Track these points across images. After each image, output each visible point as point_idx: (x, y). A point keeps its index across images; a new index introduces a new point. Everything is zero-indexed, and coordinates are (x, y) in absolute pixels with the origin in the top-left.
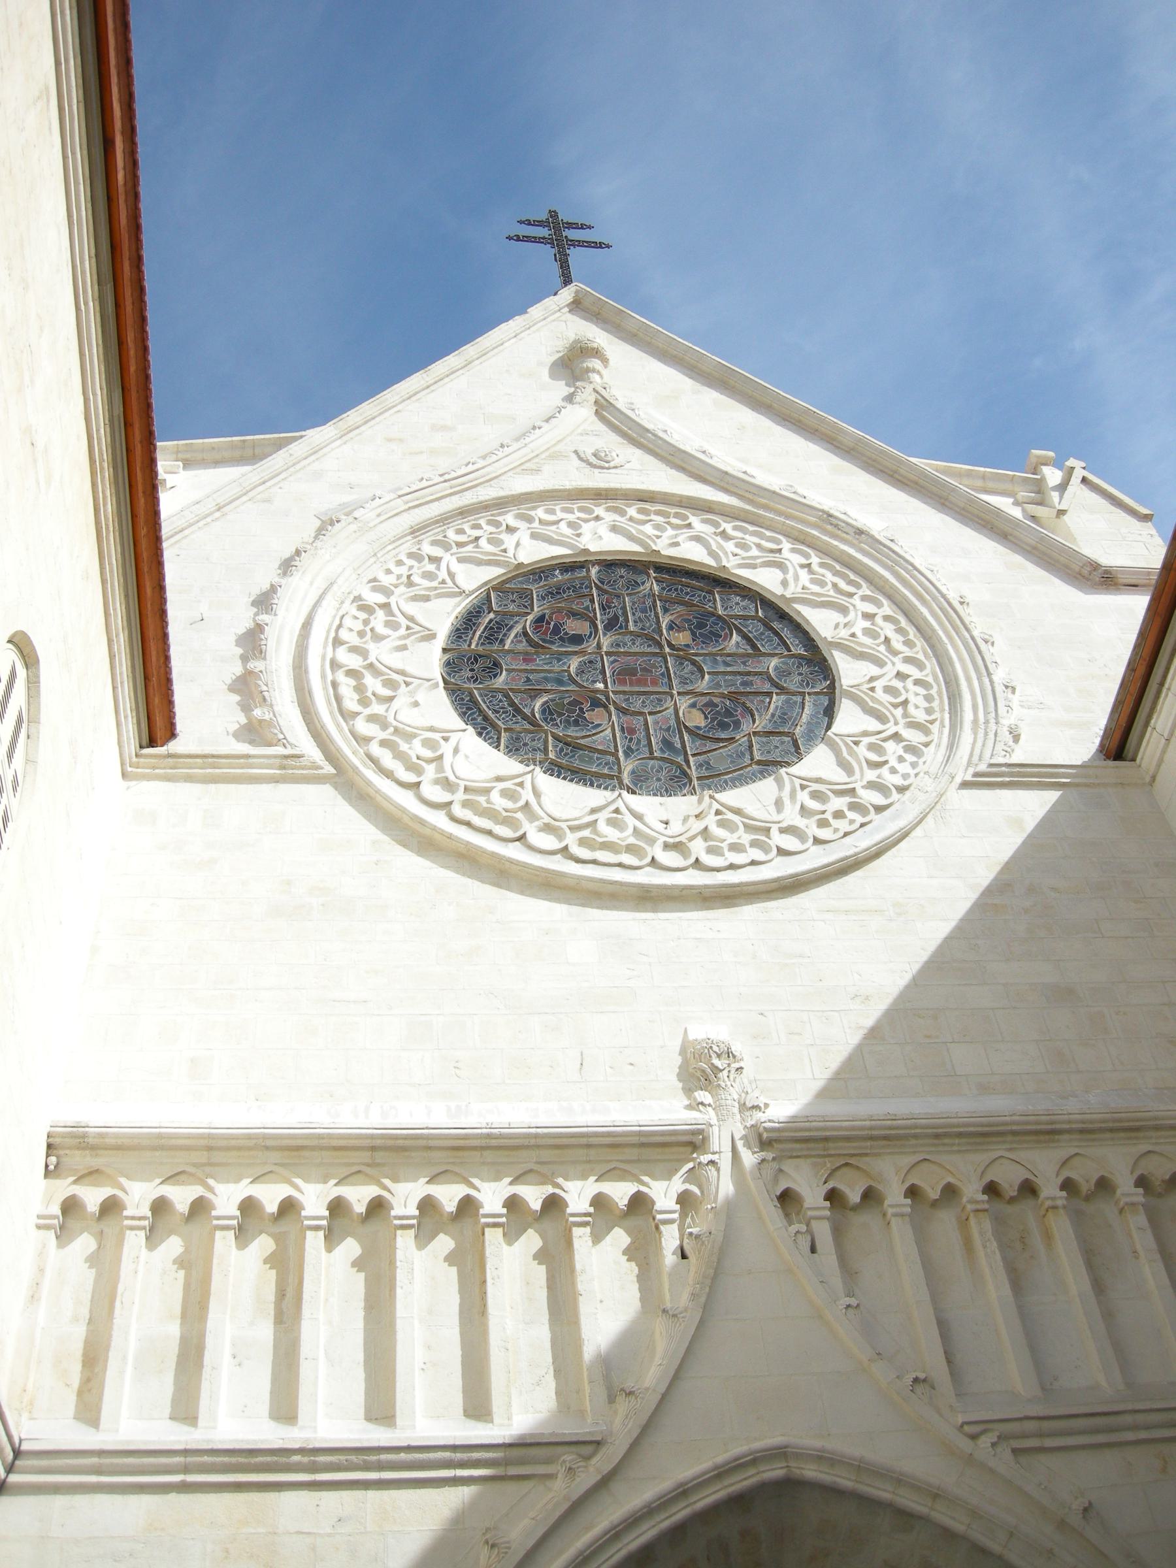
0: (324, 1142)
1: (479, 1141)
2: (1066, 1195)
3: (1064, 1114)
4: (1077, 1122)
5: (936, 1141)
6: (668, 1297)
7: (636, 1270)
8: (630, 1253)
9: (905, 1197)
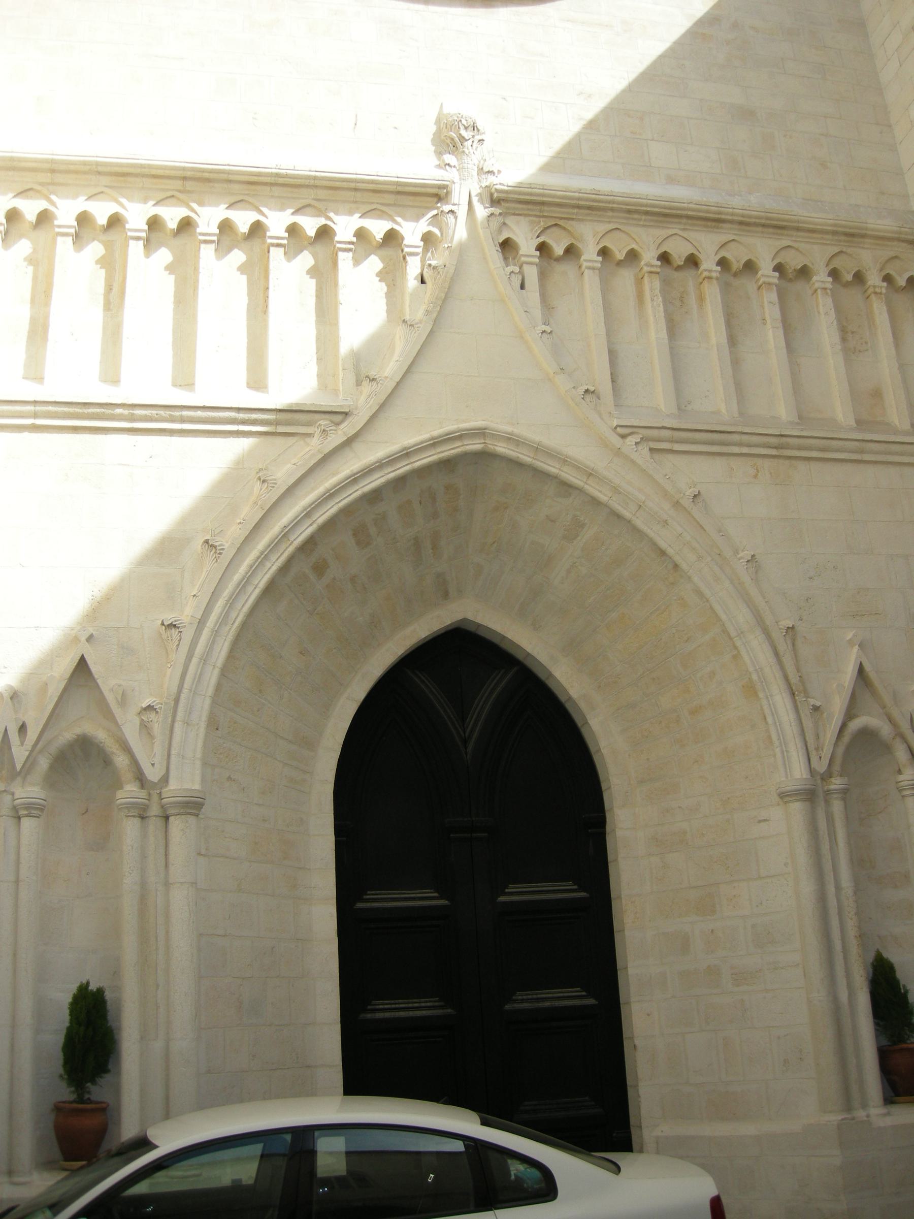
0: (146, 171)
1: (269, 178)
2: (720, 270)
3: (730, 208)
4: (738, 215)
5: (628, 216)
6: (407, 310)
7: (385, 289)
8: (382, 275)
9: (598, 255)
